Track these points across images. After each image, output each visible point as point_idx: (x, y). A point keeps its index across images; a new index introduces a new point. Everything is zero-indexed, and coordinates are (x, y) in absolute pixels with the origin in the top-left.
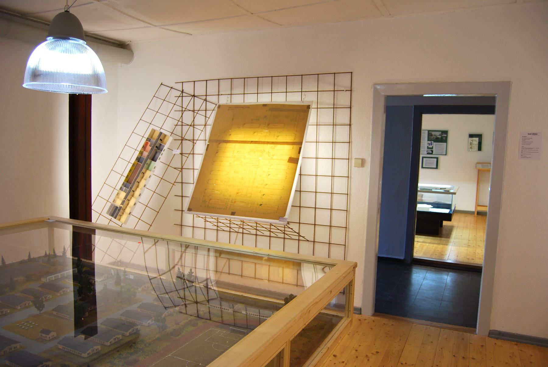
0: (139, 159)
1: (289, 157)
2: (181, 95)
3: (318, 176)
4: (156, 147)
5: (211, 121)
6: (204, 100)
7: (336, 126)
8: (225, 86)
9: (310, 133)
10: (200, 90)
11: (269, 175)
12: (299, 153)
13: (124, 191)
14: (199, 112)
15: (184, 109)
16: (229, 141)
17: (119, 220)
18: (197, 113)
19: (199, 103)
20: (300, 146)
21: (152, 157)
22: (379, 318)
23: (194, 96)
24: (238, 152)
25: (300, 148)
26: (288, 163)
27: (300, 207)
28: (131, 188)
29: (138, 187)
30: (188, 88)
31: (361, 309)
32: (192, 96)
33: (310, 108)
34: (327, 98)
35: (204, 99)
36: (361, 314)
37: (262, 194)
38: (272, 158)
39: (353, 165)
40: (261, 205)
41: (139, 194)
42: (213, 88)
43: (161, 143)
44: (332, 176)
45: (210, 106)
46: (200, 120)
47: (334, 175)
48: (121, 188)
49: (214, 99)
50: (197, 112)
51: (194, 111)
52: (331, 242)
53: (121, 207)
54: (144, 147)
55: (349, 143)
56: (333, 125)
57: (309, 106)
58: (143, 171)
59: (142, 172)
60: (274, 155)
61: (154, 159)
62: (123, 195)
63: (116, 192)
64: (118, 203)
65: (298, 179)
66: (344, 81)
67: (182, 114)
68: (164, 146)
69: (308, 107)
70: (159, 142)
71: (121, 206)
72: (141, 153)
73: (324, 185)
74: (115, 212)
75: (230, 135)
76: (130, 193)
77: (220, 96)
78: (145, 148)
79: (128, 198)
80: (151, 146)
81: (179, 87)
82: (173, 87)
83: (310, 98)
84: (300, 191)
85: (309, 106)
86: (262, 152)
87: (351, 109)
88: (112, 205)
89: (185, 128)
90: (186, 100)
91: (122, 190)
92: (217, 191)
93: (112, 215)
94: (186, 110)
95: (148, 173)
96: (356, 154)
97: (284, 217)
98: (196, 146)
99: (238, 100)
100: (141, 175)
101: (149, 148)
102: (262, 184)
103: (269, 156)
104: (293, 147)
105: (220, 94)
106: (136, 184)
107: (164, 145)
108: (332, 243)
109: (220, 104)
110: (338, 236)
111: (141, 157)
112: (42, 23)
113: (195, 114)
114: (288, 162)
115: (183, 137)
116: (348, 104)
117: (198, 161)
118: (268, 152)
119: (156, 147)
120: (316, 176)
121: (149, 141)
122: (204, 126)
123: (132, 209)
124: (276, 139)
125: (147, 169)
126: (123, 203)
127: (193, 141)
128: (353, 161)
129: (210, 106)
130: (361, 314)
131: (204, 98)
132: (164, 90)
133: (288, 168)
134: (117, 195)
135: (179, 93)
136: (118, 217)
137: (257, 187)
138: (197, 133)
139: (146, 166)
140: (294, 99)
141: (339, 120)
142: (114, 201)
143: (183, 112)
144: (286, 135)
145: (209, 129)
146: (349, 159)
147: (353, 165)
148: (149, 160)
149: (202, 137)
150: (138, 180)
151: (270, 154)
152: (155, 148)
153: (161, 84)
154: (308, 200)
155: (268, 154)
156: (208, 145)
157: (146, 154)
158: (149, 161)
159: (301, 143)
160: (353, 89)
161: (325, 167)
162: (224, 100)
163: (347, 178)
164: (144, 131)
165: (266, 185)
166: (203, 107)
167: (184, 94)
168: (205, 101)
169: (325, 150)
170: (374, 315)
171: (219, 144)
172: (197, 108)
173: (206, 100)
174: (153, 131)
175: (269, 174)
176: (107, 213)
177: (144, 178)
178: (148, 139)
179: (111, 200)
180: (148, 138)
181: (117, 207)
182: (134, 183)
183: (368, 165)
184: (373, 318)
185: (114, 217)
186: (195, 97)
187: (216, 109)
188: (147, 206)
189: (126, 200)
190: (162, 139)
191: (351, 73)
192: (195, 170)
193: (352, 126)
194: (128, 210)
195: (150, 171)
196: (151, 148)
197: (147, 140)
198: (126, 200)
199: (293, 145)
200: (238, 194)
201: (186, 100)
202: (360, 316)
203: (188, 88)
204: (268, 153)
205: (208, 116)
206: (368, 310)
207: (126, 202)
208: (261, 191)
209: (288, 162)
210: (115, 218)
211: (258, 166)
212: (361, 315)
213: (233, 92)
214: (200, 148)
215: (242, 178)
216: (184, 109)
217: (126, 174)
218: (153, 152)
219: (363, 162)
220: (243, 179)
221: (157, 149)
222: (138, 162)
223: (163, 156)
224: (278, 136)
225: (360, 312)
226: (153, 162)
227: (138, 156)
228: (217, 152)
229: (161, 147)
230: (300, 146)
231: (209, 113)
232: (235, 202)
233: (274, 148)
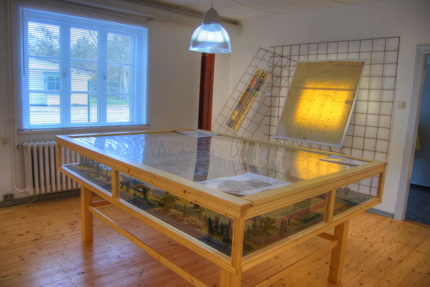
0: (248, 90)
1: (346, 100)
2: (273, 56)
3: (368, 115)
4: (260, 81)
5: (292, 74)
6: (289, 59)
7: (384, 90)
8: (304, 48)
9: (364, 82)
10: (286, 52)
11: (331, 112)
12: (354, 97)
13: (237, 110)
14: (285, 68)
15: (274, 66)
16: (304, 88)
17: (234, 129)
18: (284, 68)
19: (285, 61)
20: (354, 92)
21: (257, 89)
22: (408, 223)
23: (282, 56)
24: (310, 95)
25: (355, 94)
26: (345, 104)
27: (353, 136)
28: (242, 108)
29: (246, 108)
30: (278, 51)
31: (394, 215)
32: (281, 56)
33: (364, 64)
34: (378, 56)
35: (289, 59)
36: (393, 218)
37: (326, 126)
38: (334, 100)
39: (396, 107)
40: (325, 133)
41: (243, 118)
42: (295, 50)
43: (263, 79)
44: (379, 115)
45: (293, 63)
46: (285, 73)
47: (380, 113)
48: (235, 108)
49: (295, 58)
50: (283, 67)
51: (281, 67)
52: (379, 126)
53: (235, 121)
54: (252, 82)
55: (394, 90)
56: (382, 77)
57: (364, 62)
58: (251, 97)
59: (250, 98)
60: (335, 98)
61: (258, 90)
62: (237, 113)
63: (232, 111)
64: (234, 117)
65: (354, 107)
66: (392, 44)
67: (273, 69)
68: (265, 81)
69: (363, 63)
70: (262, 78)
71: (235, 120)
72: (250, 85)
73: (372, 120)
74: (231, 124)
75: (305, 83)
76: (241, 112)
77: (300, 56)
78: (253, 82)
79: (240, 115)
80: (256, 81)
81: (272, 50)
82: (268, 51)
83: (365, 57)
84: (354, 125)
85: (364, 62)
86: (327, 96)
87: (400, 39)
88: (229, 119)
89: (275, 79)
90: (277, 59)
91: (236, 110)
92: (295, 123)
93: (229, 126)
94: (276, 66)
95: (254, 98)
96: (399, 98)
97: (340, 143)
98: (281, 91)
99: (312, 59)
100: (249, 100)
101: (255, 82)
102: (326, 119)
103: (331, 99)
104: (349, 93)
105: (300, 54)
106: (245, 105)
107: (265, 80)
108: (377, 151)
109: (299, 62)
110: (383, 133)
111: (249, 88)
112: (187, 11)
113: (282, 69)
114: (345, 103)
115: (273, 84)
116: (395, 61)
117: (282, 102)
118: (331, 96)
119: (260, 81)
120: (366, 126)
121: (255, 78)
122: (287, 77)
123: (242, 122)
124: (337, 86)
125: (253, 96)
126: (236, 118)
127: (280, 87)
128: (396, 104)
129: (293, 63)
130: (393, 218)
131: (289, 57)
132: (262, 53)
133: (345, 108)
134: (233, 113)
135: (272, 54)
136: (233, 127)
137: (322, 121)
138: (283, 81)
139: (252, 94)
140: (353, 57)
141: (386, 86)
142: (231, 116)
143: (274, 67)
144: (345, 84)
145: (291, 79)
146: (391, 116)
147: (396, 107)
148: (254, 90)
149: (286, 85)
150: (247, 103)
151: (332, 98)
152: (259, 82)
153: (260, 48)
154: (359, 131)
155: (331, 98)
156: (290, 91)
157: (253, 86)
158: (254, 91)
159: (355, 90)
160: (400, 49)
161: (373, 107)
162: (302, 59)
163: (391, 116)
164: (252, 71)
165: (329, 119)
166: (288, 64)
167: (275, 55)
168: (290, 60)
169: (374, 95)
170: (404, 220)
171: (297, 89)
172: (284, 64)
173: (290, 59)
174: (258, 71)
175: (331, 111)
176: (226, 124)
177: (251, 101)
178: (255, 77)
179: (228, 117)
180: (254, 76)
181: (232, 121)
182: (244, 105)
183: (408, 107)
184: (403, 222)
185: (230, 127)
186: (283, 57)
187: (296, 65)
188: (252, 121)
189: (239, 116)
190: (264, 76)
191: (399, 38)
192: (280, 108)
193: (397, 78)
194: (240, 122)
195: (255, 97)
196: (256, 82)
197: (254, 77)
198: (239, 116)
199: (350, 91)
200: (309, 125)
201: (277, 59)
202: (392, 220)
203: (278, 51)
204: (331, 97)
205: (291, 70)
206: (400, 216)
207: (239, 117)
208: (325, 123)
209: (345, 103)
210: (231, 127)
211: (324, 106)
212: (393, 219)
213: (310, 53)
214: (284, 92)
215: (312, 114)
216: (274, 66)
217: (238, 100)
218: (258, 85)
219: (404, 105)
220: (313, 115)
221: (260, 83)
222: (240, 105)
223: (263, 88)
224: (339, 85)
225: (393, 217)
226: (257, 91)
227: (247, 87)
228: (296, 96)
229: (263, 81)
230: (354, 92)
231: (291, 68)
232: (307, 131)
233: (335, 93)
